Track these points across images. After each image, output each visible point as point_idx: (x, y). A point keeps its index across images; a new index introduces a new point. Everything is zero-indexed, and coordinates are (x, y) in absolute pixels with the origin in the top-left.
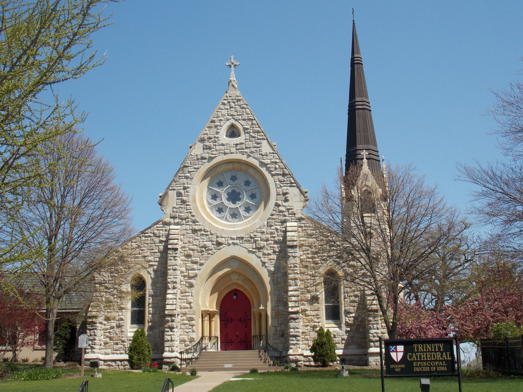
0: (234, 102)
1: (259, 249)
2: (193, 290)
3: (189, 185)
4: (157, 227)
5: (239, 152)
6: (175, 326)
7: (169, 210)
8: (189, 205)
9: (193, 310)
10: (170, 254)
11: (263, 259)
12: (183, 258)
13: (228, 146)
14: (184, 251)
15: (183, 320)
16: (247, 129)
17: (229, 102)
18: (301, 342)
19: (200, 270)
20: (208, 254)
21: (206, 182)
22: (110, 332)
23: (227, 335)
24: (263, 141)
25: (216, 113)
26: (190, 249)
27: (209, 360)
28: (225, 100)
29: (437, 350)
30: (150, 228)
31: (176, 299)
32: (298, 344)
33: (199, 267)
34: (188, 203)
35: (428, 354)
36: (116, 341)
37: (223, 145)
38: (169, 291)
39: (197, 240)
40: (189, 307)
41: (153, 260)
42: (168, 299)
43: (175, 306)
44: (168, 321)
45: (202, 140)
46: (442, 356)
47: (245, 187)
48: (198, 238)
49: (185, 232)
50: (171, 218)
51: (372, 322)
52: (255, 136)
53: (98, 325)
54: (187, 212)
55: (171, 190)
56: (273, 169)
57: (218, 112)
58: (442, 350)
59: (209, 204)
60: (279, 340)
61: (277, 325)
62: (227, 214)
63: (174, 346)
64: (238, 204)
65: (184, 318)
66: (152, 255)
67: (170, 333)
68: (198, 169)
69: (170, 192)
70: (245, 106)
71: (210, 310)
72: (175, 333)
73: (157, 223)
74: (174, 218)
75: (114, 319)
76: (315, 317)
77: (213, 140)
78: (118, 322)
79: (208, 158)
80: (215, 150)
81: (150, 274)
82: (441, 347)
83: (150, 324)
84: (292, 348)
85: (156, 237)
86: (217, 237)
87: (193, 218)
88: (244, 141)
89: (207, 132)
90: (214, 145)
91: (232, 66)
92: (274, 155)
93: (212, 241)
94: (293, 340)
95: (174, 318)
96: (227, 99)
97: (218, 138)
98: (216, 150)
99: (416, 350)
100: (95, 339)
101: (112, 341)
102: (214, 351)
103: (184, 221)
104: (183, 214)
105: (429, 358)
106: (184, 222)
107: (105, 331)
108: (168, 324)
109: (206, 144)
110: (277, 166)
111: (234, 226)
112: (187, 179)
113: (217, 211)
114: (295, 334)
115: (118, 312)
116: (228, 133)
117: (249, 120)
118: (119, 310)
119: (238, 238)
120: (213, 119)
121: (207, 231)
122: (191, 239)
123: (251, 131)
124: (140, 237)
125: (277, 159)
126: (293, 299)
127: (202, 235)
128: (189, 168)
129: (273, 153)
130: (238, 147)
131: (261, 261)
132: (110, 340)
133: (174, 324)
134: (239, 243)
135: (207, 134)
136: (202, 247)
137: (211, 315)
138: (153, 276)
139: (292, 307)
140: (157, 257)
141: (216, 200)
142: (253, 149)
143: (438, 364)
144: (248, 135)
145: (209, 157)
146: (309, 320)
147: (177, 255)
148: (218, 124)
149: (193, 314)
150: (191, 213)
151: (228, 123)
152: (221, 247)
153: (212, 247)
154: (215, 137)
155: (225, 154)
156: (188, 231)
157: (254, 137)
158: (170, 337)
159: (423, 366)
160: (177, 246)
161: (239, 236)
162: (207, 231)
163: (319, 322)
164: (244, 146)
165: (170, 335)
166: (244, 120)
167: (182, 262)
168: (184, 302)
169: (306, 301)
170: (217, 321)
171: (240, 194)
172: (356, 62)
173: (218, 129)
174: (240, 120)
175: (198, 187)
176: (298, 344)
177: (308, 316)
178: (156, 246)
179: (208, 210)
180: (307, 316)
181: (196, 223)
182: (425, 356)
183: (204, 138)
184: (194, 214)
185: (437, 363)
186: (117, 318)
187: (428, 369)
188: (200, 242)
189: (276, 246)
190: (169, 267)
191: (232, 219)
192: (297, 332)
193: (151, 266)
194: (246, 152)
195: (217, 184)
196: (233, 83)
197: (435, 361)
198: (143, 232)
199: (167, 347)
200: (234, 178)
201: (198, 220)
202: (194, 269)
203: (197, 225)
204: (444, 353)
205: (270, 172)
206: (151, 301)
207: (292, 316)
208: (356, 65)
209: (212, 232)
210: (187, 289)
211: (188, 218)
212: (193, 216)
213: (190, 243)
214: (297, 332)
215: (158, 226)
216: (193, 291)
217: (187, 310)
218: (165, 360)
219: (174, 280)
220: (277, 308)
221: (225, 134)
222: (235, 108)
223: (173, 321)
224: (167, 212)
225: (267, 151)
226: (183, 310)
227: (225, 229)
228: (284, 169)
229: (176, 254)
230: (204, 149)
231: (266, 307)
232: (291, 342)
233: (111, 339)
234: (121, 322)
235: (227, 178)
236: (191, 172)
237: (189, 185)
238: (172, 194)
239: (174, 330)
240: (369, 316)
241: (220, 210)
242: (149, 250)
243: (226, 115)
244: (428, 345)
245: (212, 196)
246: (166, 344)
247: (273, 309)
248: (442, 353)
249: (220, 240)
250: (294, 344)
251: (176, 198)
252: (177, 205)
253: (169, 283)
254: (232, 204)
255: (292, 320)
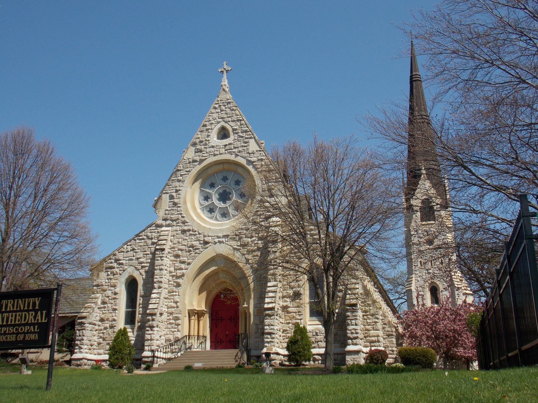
0: (224, 106)
1: (244, 245)
2: (180, 289)
3: (180, 188)
4: (150, 230)
5: (228, 152)
6: (155, 325)
7: (161, 213)
8: (180, 207)
9: (179, 310)
10: (157, 254)
11: (246, 256)
12: (173, 258)
13: (218, 147)
14: (174, 251)
15: (170, 319)
16: (236, 129)
17: (220, 106)
18: (276, 340)
19: (187, 269)
20: (196, 253)
21: (198, 184)
22: (103, 333)
23: (217, 334)
24: (251, 140)
25: (208, 117)
26: (179, 250)
27: (185, 360)
28: (216, 104)
29: (31, 308)
30: (144, 231)
31: (159, 298)
32: (272, 342)
33: (186, 266)
34: (179, 205)
35: (18, 314)
36: (108, 342)
37: (213, 147)
38: (155, 291)
39: (186, 240)
40: (175, 306)
41: (145, 262)
42: (152, 298)
43: (157, 305)
44: (149, 320)
45: (194, 144)
46: (35, 317)
47: (234, 186)
48: (187, 238)
49: (175, 233)
50: (163, 220)
51: (350, 318)
52: (243, 135)
53: (86, 325)
54: (178, 214)
55: (164, 193)
56: (259, 166)
57: (210, 116)
58: (37, 308)
59: (201, 205)
60: (260, 339)
61: (258, 323)
62: (217, 214)
63: (153, 346)
64: (229, 203)
65: (171, 317)
66: (144, 257)
67: (150, 332)
68: (189, 171)
69: (164, 196)
70: (234, 108)
71: (197, 309)
72: (155, 332)
73: (150, 226)
74: (165, 220)
75: (108, 319)
76: (297, 314)
77: (204, 143)
78: (111, 323)
79: (198, 160)
80: (205, 152)
81: (142, 275)
82: (37, 303)
83: (139, 324)
84: (266, 346)
85: (149, 239)
86: (204, 236)
87: (183, 219)
88: (233, 141)
89: (199, 136)
90: (205, 148)
91: (225, 72)
92: (261, 152)
93: (199, 240)
94: (268, 338)
95: (154, 317)
96: (218, 103)
97: (209, 141)
98: (207, 153)
99: (4, 310)
100: (83, 340)
101: (105, 342)
102: (200, 350)
103: (174, 222)
104: (174, 216)
105: (19, 321)
106: (175, 223)
107: (99, 332)
108: (148, 323)
109: (197, 147)
110: (263, 163)
111: (221, 225)
112: (179, 182)
113: (209, 211)
114: (270, 331)
115: (111, 313)
116: (220, 135)
117: (238, 120)
118: (113, 311)
119: (224, 236)
120: (205, 123)
121: (195, 231)
122: (180, 240)
123: (240, 131)
124: (135, 240)
125: (264, 156)
126: (271, 294)
127: (191, 235)
128: (181, 171)
129: (260, 151)
130: (227, 148)
131: (246, 258)
132: (103, 341)
133: (155, 323)
134: (224, 241)
135: (199, 138)
136: (190, 247)
137: (199, 314)
138: (144, 277)
139: (268, 303)
140: (149, 258)
141: (207, 201)
142: (240, 149)
143: (28, 330)
144: (237, 135)
145: (200, 160)
146: (291, 317)
147: (164, 255)
148: (210, 127)
149: (179, 314)
150: (181, 214)
151: (219, 126)
152: (208, 245)
153: (199, 246)
154: (206, 140)
155: (215, 155)
156: (177, 232)
157: (242, 137)
158: (150, 336)
159: (9, 334)
160: (164, 247)
161: (224, 234)
162: (195, 231)
163: (301, 320)
164: (232, 146)
165: (150, 334)
166: (233, 121)
167: (171, 263)
168: (171, 302)
169: (287, 298)
170: (206, 321)
171: (230, 193)
172: (414, 79)
173: (209, 132)
174: (229, 121)
175: (189, 189)
176: (272, 342)
177: (290, 313)
178: (148, 248)
179: (199, 211)
180: (288, 312)
181: (186, 224)
182: (13, 318)
183: (195, 142)
184: (184, 215)
185: (27, 328)
186: (111, 319)
187: (13, 338)
188: (188, 242)
189: (260, 242)
190: (156, 267)
191: (221, 219)
192: (272, 329)
193: (143, 267)
194: (234, 152)
195: (210, 185)
196: (224, 87)
197: (25, 325)
198: (137, 235)
199: (146, 346)
200: (225, 179)
201: (187, 221)
202: (181, 269)
203: (186, 226)
204: (39, 313)
205: (256, 169)
206: (141, 301)
207: (267, 312)
208: (414, 82)
209: (199, 231)
210: (175, 289)
211: (178, 219)
212: (183, 217)
213: (179, 244)
214: (272, 329)
215: (151, 228)
216: (180, 290)
217: (173, 309)
218: (144, 359)
219: (160, 280)
220: (259, 305)
221: (216, 136)
222: (225, 111)
223: (153, 320)
224: (160, 215)
225: (254, 150)
226: (170, 309)
227: (212, 228)
228: (269, 165)
229: (163, 254)
230: (195, 152)
231: (248, 304)
232: (266, 340)
233: (104, 339)
234: (114, 322)
235: (218, 179)
236: (183, 175)
237: (180, 188)
238: (165, 197)
239: (154, 329)
240: (347, 310)
241: (211, 210)
242: (142, 252)
243: (217, 118)
244: (20, 301)
245: (205, 197)
246: (146, 343)
247: (255, 307)
248: (36, 311)
249: (206, 239)
250: (268, 342)
251: (168, 200)
252: (169, 207)
253: (155, 283)
254: (222, 204)
255: (267, 317)
